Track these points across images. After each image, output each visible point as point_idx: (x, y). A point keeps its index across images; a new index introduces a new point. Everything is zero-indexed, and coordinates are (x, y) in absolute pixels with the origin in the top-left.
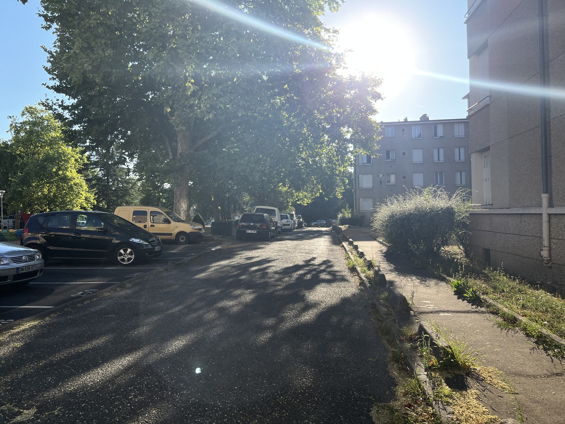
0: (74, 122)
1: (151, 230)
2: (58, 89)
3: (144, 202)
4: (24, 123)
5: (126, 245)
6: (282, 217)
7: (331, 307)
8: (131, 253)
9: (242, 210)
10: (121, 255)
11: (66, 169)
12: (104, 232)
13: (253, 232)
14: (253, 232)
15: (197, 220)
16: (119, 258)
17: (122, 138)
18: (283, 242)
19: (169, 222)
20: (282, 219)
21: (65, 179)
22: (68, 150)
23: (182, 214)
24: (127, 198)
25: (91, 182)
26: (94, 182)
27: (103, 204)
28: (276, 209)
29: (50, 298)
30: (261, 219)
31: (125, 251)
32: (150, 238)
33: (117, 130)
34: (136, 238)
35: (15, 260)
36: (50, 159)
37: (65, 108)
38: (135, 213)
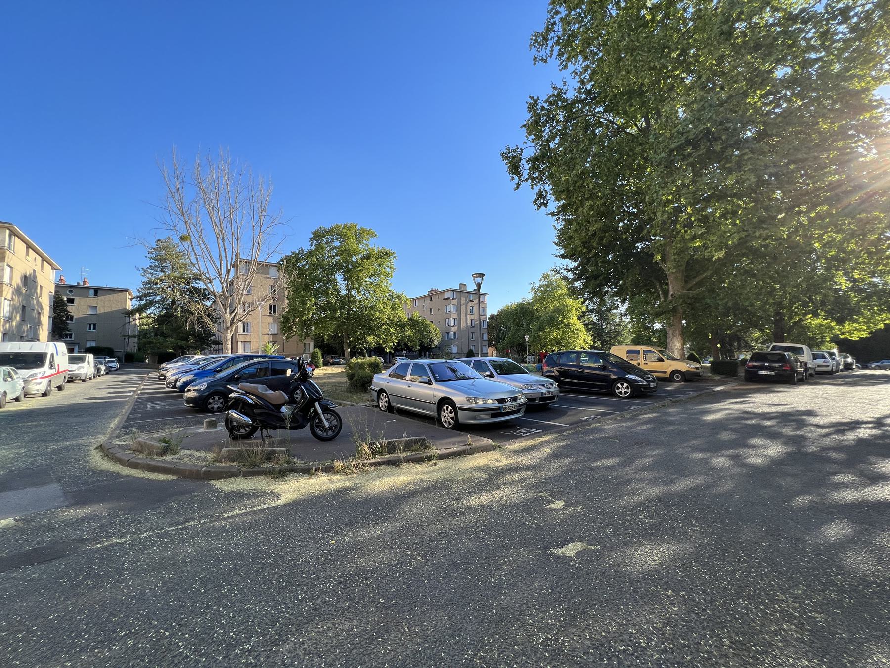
0: (575, 280)
1: (645, 368)
2: (563, 257)
3: (636, 342)
4: (541, 286)
5: (624, 380)
6: (815, 357)
7: (367, 498)
8: (627, 388)
9: (750, 348)
10: (618, 388)
11: (569, 317)
12: (604, 368)
13: (769, 373)
14: (769, 373)
15: (692, 358)
16: (617, 391)
17: (615, 288)
18: (820, 387)
19: (663, 361)
20: (814, 359)
21: (568, 325)
22: (569, 302)
23: (676, 352)
24: (619, 339)
25: (590, 327)
26: (590, 326)
27: (598, 344)
28: (804, 347)
29: (564, 418)
30: (782, 359)
31: (622, 385)
32: (645, 375)
33: (610, 281)
34: (631, 374)
35: (541, 387)
36: (558, 311)
37: (568, 270)
38: (629, 352)
